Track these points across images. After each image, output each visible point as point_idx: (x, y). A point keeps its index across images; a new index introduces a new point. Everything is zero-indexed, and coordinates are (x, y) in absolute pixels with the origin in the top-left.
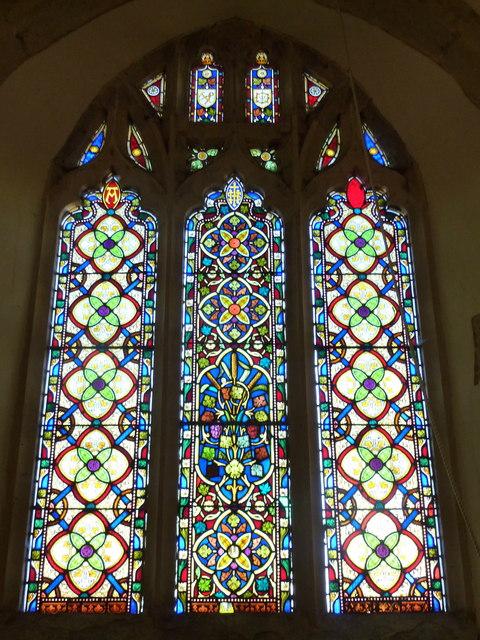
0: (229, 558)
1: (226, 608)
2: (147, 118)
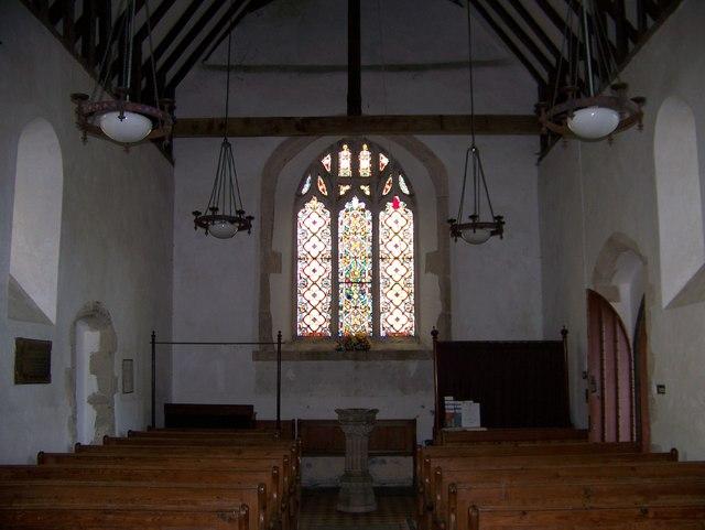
0: (355, 322)
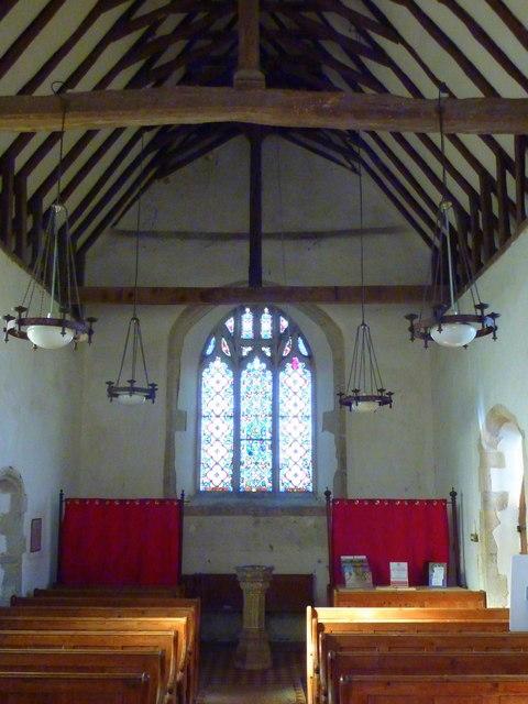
0: (255, 477)
1: (254, 490)
2: (20, 309)
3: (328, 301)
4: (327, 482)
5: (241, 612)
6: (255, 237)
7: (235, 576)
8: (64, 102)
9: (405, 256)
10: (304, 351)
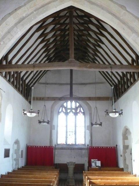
0: (71, 141)
3: (88, 100)
4: (88, 142)
5: (68, 172)
6: (71, 84)
7: (67, 164)
8: (34, 66)
9: (107, 89)
10: (82, 111)
